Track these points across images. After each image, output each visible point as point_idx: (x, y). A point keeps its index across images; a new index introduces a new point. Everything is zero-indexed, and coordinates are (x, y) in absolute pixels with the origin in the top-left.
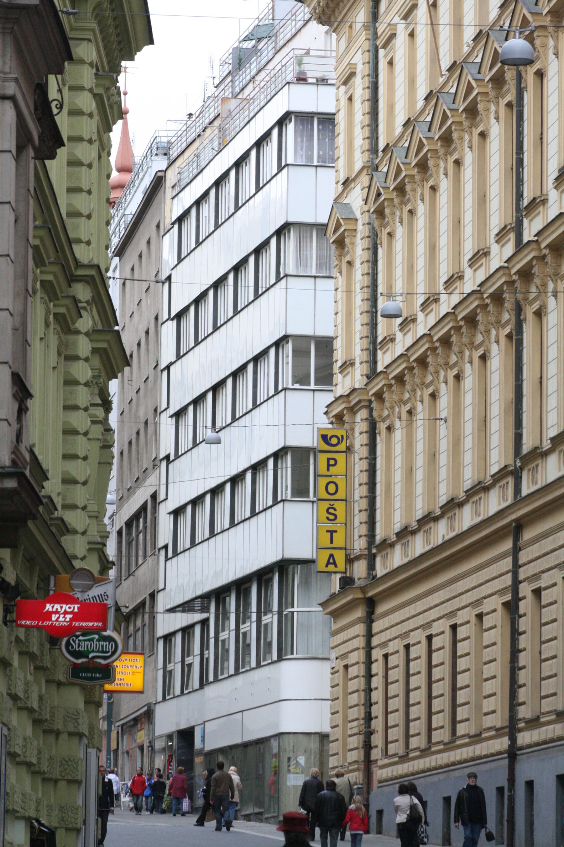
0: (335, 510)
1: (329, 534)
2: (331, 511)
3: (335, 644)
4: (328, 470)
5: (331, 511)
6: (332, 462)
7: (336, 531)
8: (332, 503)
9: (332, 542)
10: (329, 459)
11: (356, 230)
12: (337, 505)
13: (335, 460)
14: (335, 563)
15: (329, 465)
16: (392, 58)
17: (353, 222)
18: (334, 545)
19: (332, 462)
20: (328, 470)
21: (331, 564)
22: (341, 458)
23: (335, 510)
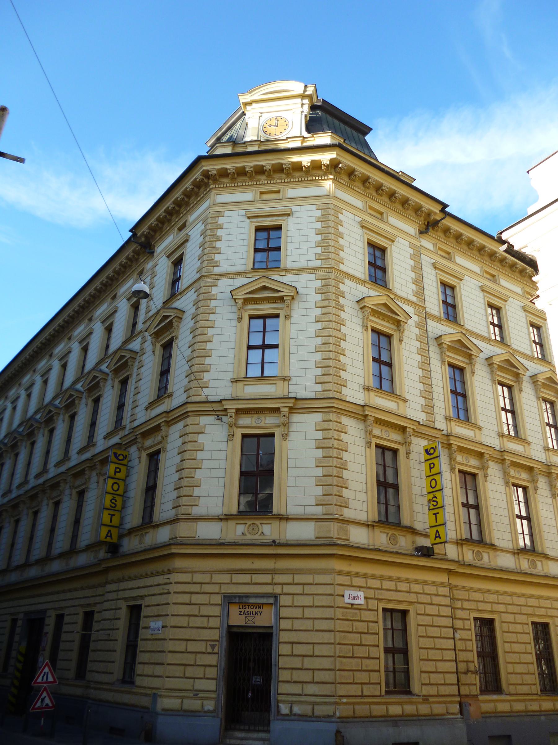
0: (116, 501)
1: (110, 516)
2: (113, 501)
3: (177, 591)
4: (115, 474)
5: (113, 501)
6: (118, 470)
7: (438, 513)
8: (434, 494)
9: (436, 522)
10: (116, 468)
11: (181, 318)
12: (118, 498)
13: (433, 464)
14: (111, 537)
15: (116, 472)
16: (186, 221)
17: (182, 313)
18: (113, 524)
19: (118, 470)
20: (115, 474)
21: (109, 536)
22: (123, 469)
23: (116, 501)
